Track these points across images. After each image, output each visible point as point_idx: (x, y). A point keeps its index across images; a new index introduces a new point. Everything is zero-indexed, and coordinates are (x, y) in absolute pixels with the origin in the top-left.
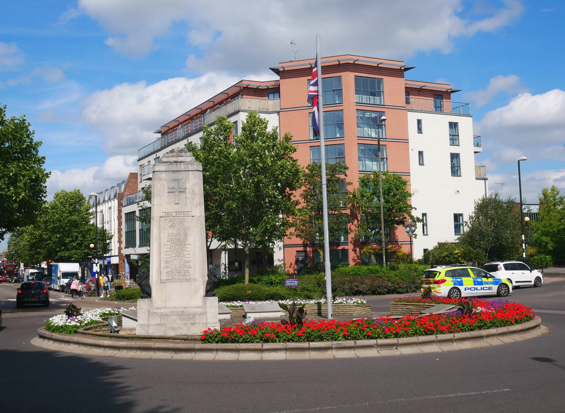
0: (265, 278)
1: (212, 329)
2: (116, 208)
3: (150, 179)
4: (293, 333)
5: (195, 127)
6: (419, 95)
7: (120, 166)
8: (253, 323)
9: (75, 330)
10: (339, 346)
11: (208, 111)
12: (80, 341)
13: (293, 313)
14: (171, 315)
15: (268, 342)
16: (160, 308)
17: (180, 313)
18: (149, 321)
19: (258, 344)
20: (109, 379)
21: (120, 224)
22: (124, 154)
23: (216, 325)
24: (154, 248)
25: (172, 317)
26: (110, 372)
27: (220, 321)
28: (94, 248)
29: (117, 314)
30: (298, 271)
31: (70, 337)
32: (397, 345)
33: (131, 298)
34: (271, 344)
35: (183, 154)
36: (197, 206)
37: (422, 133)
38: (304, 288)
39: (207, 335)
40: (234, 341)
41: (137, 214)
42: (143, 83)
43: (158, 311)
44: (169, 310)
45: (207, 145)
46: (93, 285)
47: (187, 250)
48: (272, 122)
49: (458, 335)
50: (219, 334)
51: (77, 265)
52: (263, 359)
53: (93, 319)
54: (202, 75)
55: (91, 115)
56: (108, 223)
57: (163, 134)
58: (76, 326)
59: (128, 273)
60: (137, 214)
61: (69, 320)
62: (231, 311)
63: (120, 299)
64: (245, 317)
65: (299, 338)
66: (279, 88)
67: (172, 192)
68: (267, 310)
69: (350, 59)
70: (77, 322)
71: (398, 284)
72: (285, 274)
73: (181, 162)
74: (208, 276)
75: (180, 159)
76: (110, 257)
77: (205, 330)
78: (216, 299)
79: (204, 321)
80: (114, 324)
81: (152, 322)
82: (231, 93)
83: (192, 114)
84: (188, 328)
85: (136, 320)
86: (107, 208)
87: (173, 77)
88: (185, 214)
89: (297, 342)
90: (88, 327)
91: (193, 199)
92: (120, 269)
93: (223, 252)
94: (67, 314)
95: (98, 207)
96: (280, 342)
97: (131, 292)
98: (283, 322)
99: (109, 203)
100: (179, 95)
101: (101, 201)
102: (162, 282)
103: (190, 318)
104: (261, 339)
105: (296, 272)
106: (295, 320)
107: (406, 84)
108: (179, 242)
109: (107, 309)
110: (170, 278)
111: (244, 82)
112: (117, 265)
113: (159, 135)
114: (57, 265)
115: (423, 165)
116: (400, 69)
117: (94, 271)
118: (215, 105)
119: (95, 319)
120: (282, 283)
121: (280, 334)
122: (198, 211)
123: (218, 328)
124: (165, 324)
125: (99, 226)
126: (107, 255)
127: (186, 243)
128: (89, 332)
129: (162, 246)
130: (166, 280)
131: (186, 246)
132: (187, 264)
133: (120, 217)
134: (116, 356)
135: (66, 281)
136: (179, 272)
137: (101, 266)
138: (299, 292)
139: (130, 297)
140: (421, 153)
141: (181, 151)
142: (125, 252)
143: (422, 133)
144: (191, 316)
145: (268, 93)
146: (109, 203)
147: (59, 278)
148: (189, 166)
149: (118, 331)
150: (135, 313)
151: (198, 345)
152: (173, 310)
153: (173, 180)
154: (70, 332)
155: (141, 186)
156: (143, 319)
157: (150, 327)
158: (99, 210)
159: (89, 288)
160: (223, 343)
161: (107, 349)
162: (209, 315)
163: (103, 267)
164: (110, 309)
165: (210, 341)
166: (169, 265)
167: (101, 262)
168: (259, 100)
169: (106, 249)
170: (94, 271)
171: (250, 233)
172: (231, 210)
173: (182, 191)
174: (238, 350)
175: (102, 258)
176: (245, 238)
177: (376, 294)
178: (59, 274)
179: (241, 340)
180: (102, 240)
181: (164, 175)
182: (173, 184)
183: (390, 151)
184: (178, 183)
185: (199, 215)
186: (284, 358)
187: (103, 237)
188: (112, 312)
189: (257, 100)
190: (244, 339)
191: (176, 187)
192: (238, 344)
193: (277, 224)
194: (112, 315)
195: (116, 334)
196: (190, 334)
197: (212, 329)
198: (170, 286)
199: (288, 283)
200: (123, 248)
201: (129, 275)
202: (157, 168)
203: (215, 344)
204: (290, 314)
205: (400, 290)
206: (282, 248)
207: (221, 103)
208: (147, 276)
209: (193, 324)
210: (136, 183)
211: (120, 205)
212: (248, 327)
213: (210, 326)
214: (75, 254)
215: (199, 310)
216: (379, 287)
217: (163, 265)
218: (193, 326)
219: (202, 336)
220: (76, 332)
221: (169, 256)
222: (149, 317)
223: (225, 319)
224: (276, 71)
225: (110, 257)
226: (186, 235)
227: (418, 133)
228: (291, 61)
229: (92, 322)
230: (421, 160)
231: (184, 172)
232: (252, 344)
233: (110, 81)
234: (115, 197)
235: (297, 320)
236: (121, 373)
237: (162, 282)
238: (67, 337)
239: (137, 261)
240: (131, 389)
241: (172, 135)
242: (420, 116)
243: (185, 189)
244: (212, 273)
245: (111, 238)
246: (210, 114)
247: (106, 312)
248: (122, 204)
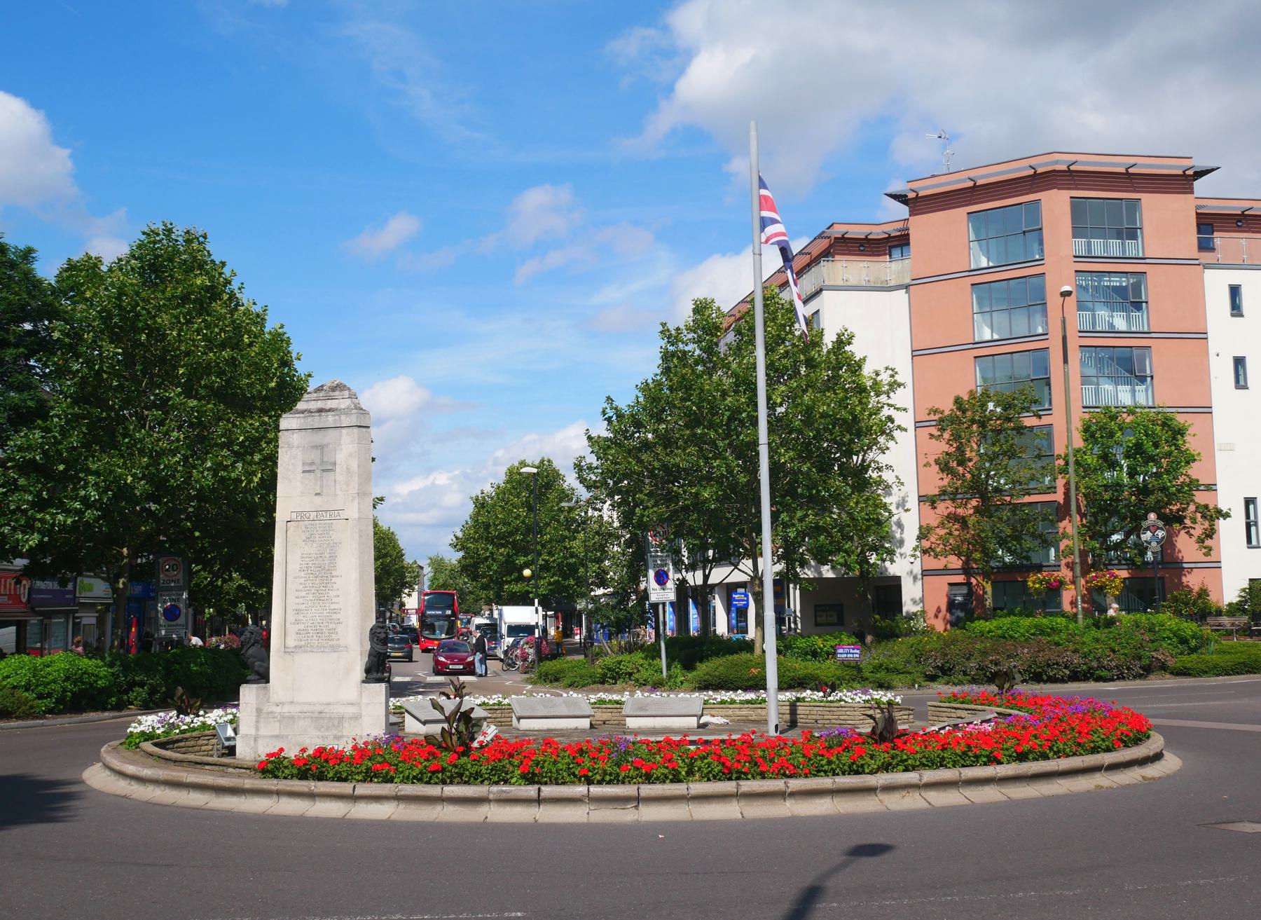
6: (1239, 229)
10: (504, 796)
16: (283, 704)
32: (638, 800)
35: (337, 393)
36: (354, 498)
37: (1242, 316)
38: (881, 666)
43: (278, 710)
44: (298, 708)
46: (531, 651)
47: (335, 587)
49: (796, 784)
65: (460, 777)
69: (1057, 162)
71: (1098, 659)
73: (329, 410)
75: (330, 404)
91: (348, 485)
102: (286, 651)
107: (1198, 207)
108: (322, 573)
115: (1245, 387)
116: (1184, 174)
131: (334, 580)
132: (334, 616)
136: (319, 632)
140: (1239, 362)
143: (1242, 316)
144: (336, 723)
145: (891, 247)
148: (343, 417)
152: (305, 708)
153: (313, 447)
157: (260, 741)
161: (133, 782)
166: (301, 617)
168: (865, 264)
173: (328, 468)
177: (1045, 682)
182: (314, 456)
183: (1160, 359)
184: (322, 453)
189: (861, 264)
190: (337, 772)
205: (1104, 673)
215: (351, 710)
216: (1049, 665)
217: (291, 617)
221: (301, 600)
222: (257, 722)
226: (333, 557)
227: (1233, 315)
228: (933, 176)
230: (1241, 378)
242: (1235, 277)
243: (335, 464)
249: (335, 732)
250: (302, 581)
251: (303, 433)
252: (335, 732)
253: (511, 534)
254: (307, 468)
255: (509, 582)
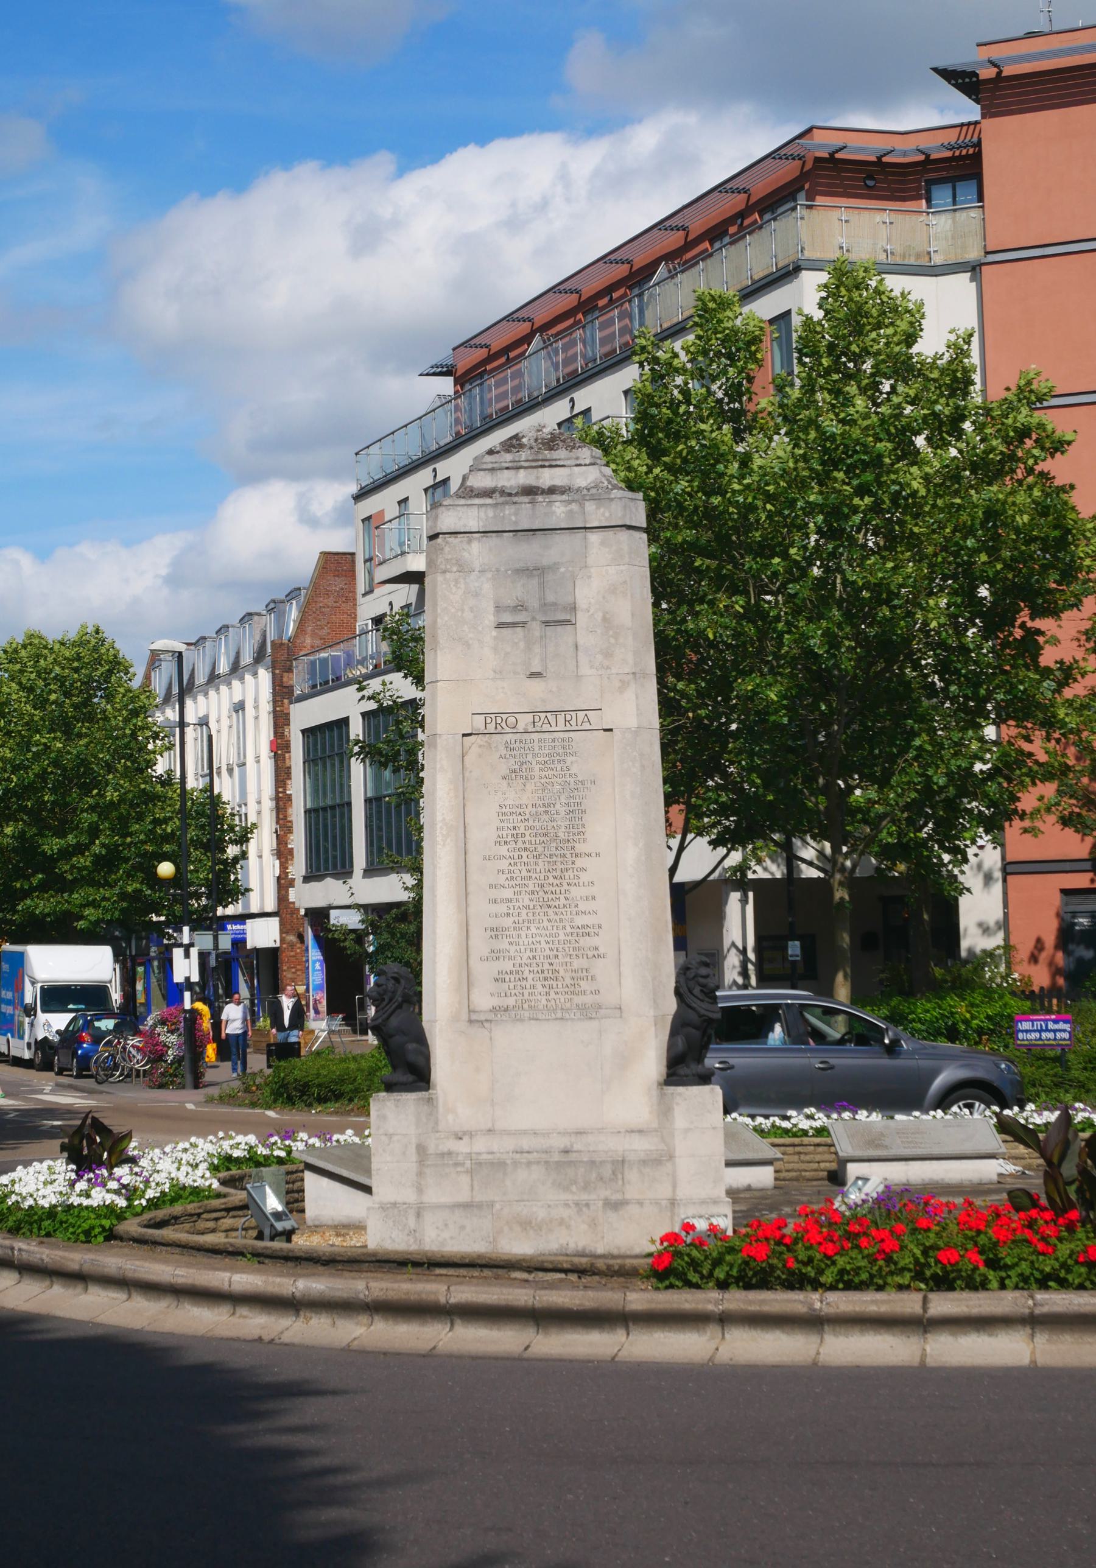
0: (925, 1009)
1: (701, 1225)
2: (266, 707)
3: (414, 578)
4: (1064, 1250)
5: (603, 342)
7: (279, 528)
8: (879, 1200)
9: (106, 1228)
11: (662, 271)
12: (130, 1275)
13: (1062, 1158)
14: (516, 1164)
15: (951, 1288)
16: (471, 1134)
17: (556, 1157)
18: (420, 1190)
19: (904, 1295)
20: (263, 1436)
21: (282, 775)
22: (294, 475)
23: (714, 1209)
24: (440, 873)
25: (522, 1174)
26: (271, 1405)
27: (733, 1194)
28: (177, 880)
29: (280, 1161)
30: (1069, 976)
31: (89, 1256)
33: (338, 1097)
34: (966, 1295)
35: (561, 454)
36: (623, 686)
39: (678, 1254)
40: (796, 1282)
41: (356, 729)
42: (384, 161)
43: (462, 1147)
44: (509, 1144)
45: (656, 426)
46: (173, 1038)
48: (945, 314)
50: (731, 1250)
51: (104, 953)
52: (930, 1362)
53: (183, 1179)
54: (640, 121)
55: (158, 302)
56: (230, 771)
57: (460, 381)
58: (110, 1210)
59: (318, 988)
60: (356, 729)
61: (81, 1185)
62: (776, 1153)
63: (290, 1101)
64: (837, 1178)
66: (976, 159)
67: (513, 625)
68: (936, 1151)
70: (117, 1192)
72: (1013, 994)
73: (552, 490)
74: (678, 993)
75: (547, 478)
76: (242, 918)
77: (666, 1230)
78: (712, 1095)
79: (663, 1191)
80: (273, 1203)
81: (432, 1196)
82: (760, 187)
83: (589, 287)
84: (593, 1224)
85: (367, 1189)
86: (226, 706)
87: (512, 129)
88: (575, 719)
89: (1081, 1287)
90: (160, 1214)
91: (608, 654)
92: (286, 973)
93: (735, 897)
94: (70, 1160)
95: (189, 703)
96: (1003, 1287)
97: (337, 1069)
98: (1021, 1199)
99: (236, 683)
100: (533, 207)
101: (201, 679)
102: (474, 1020)
103: (601, 1179)
104: (919, 1276)
105: (1061, 981)
106: (1072, 1191)
108: (550, 847)
109: (240, 1138)
110: (511, 1001)
111: (819, 137)
112: (271, 956)
113: (446, 385)
114: (21, 955)
117: (178, 977)
118: (688, 245)
119: (188, 1182)
120: (1001, 1028)
121: (1003, 1252)
122: (632, 709)
123: (725, 1223)
124: (491, 1205)
125: (193, 783)
126: (230, 910)
127: (580, 848)
128: (168, 1233)
129: (474, 859)
130: (494, 1010)
131: (580, 862)
132: (585, 942)
133: (280, 747)
134: (286, 1338)
135: (59, 1021)
137: (203, 956)
138: (1075, 1073)
139: (338, 1092)
141: (551, 443)
142: (308, 896)
144: (607, 1171)
145: (930, 183)
146: (236, 683)
147: (30, 1011)
148: (590, 506)
149: (288, 1235)
150: (361, 1156)
151: (640, 1298)
152: (526, 1143)
154: (87, 1233)
155: (368, 608)
156: (398, 1183)
157: (428, 1217)
158: (190, 717)
159: (156, 1054)
160: (748, 1287)
161: (243, 1311)
162: (684, 1166)
163: (213, 962)
164: (252, 1139)
165: (694, 1278)
166: (503, 944)
167: (205, 941)
168: (886, 217)
169: (225, 886)
170: (178, 977)
171: (853, 811)
172: (763, 714)
173: (559, 618)
174: (815, 1322)
175: (206, 922)
176: (828, 828)
178: (30, 994)
179: (828, 1278)
180: (206, 847)
181: (476, 552)
184: (542, 586)
185: (633, 722)
186: (1026, 1361)
187: (211, 829)
188: (262, 1151)
189: (879, 217)
190: (842, 1272)
191: (534, 603)
192: (815, 1296)
193: (978, 767)
194: (258, 1164)
195: (278, 1245)
196: (600, 1250)
197: (701, 1225)
198: (508, 1038)
199: (1029, 1031)
200: (299, 881)
201: (322, 997)
202: (448, 520)
203: (715, 1294)
204: (1049, 1162)
206: (998, 875)
207: (717, 233)
208: (407, 992)
209: (614, 1206)
210: (348, 597)
211: (282, 694)
212: (860, 1220)
213: (685, 1214)
214: (94, 904)
215: (640, 1146)
217: (480, 944)
218: (612, 1216)
219: (660, 1255)
220: (111, 1236)
221: (503, 908)
222: (420, 1174)
223: (749, 1188)
224: (963, 80)
225: (242, 918)
226: (576, 814)
228: (1031, 35)
229: (180, 1192)
231: (565, 537)
232: (880, 1296)
233: (240, 154)
234: (259, 658)
235: (1079, 1191)
236: (311, 1410)
237: (474, 1020)
238: (76, 1258)
239: (359, 936)
240: (354, 1478)
241: (504, 381)
243: (574, 608)
244: (695, 978)
245: (243, 839)
246: (669, 286)
247: (236, 1153)
248: (290, 690)
249: (605, 1193)
250: (504, 864)
251: (494, 540)
252: (605, 1193)
253: (28, 789)
254: (508, 618)
255: (26, 894)
